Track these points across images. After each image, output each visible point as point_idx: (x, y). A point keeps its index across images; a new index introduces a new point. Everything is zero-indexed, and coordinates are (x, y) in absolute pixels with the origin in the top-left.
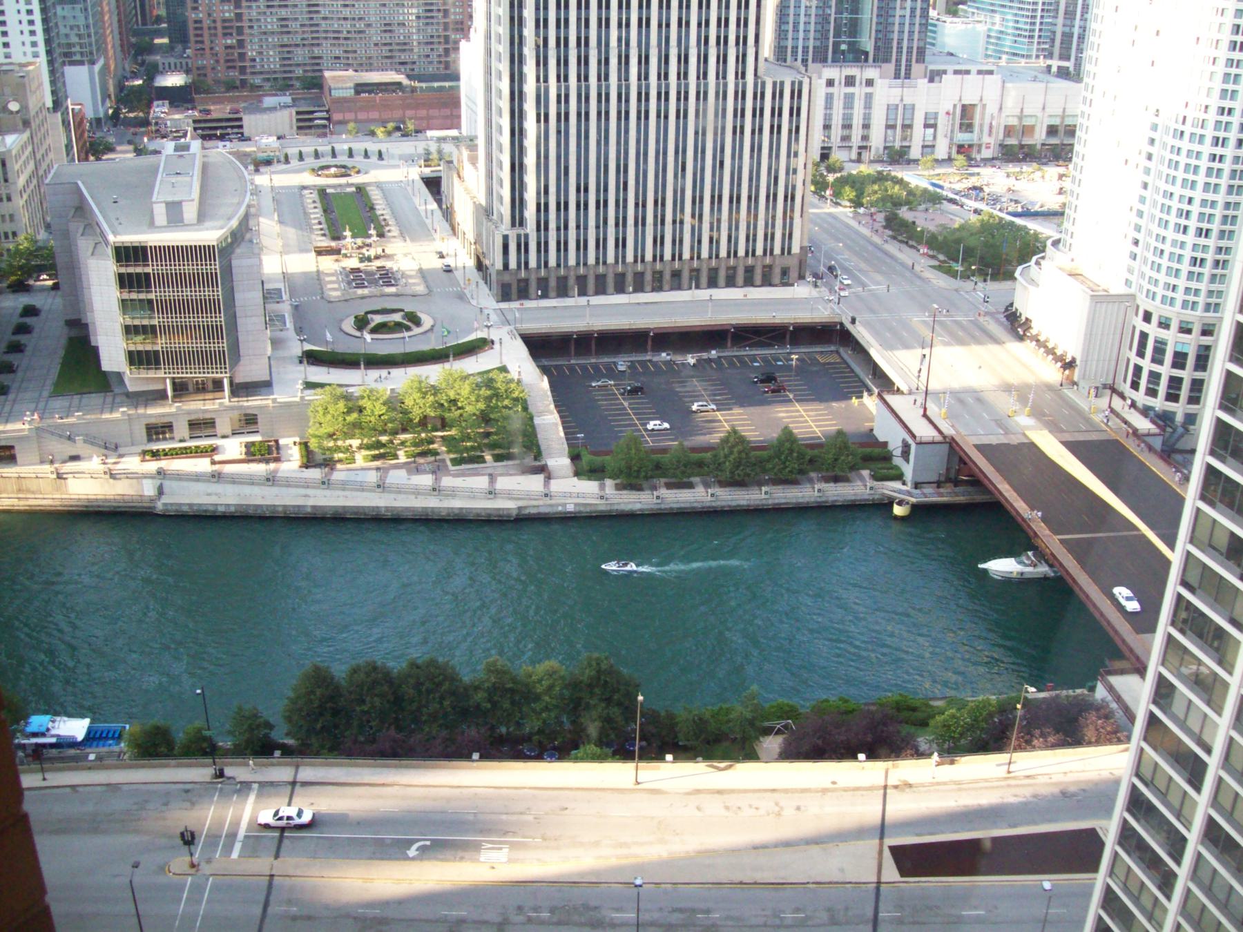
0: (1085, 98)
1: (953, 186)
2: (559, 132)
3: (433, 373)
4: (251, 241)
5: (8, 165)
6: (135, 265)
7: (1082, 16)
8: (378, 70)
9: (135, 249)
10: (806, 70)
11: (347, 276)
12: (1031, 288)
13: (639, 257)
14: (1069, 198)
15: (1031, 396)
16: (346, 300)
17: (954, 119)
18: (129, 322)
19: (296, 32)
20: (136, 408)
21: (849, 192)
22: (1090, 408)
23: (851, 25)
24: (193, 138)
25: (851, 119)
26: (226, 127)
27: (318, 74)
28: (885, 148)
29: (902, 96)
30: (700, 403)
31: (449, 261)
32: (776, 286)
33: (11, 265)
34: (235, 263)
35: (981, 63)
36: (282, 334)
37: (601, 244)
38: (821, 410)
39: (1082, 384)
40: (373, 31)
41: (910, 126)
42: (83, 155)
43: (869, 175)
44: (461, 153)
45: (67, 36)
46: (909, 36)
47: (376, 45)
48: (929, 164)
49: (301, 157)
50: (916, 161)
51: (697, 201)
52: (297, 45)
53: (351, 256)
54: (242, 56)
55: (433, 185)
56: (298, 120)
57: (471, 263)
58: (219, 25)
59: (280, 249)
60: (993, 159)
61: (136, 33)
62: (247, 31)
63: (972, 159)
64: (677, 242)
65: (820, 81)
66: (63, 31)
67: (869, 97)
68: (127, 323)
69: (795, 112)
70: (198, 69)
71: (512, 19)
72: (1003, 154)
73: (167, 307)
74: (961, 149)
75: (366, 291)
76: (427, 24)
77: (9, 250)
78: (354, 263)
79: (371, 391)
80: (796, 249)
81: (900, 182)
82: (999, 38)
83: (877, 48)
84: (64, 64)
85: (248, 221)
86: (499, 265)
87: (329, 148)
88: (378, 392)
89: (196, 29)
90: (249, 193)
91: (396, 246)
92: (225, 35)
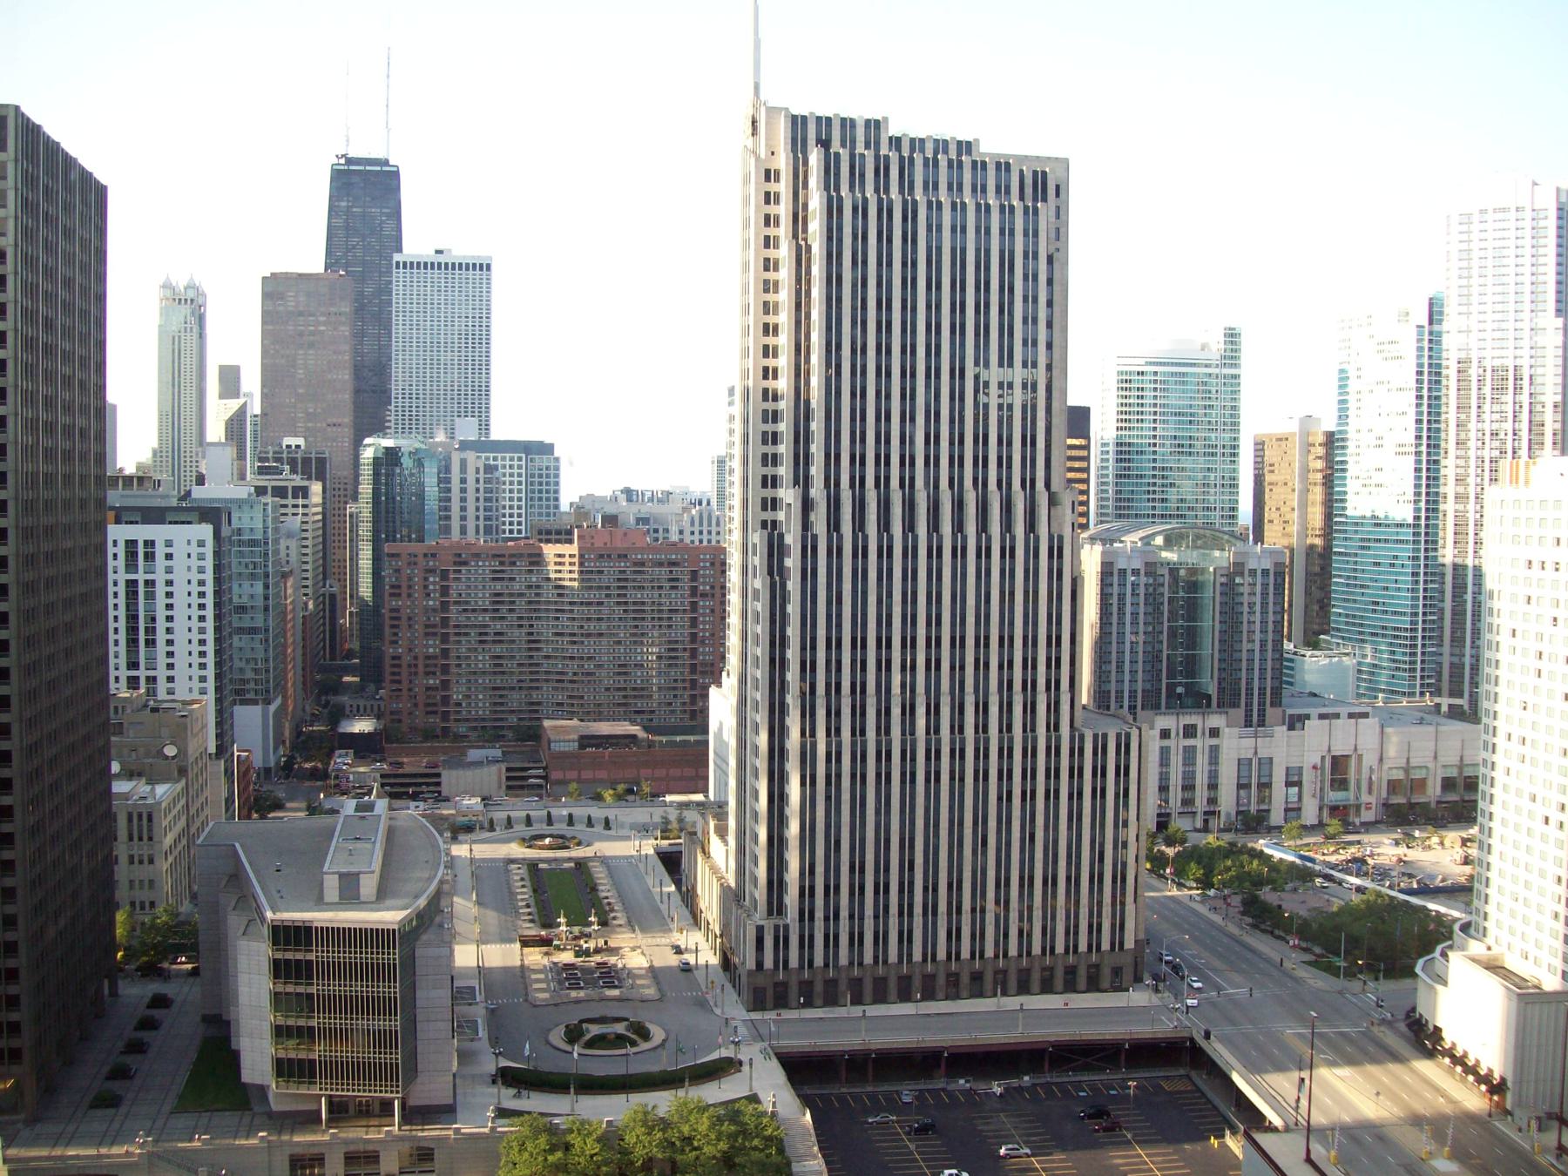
0: (1486, 743)
1: (1327, 858)
2: (828, 798)
3: (663, 1102)
4: (441, 926)
5: (155, 820)
6: (296, 950)
7: (1473, 642)
8: (608, 720)
9: (297, 929)
10: (1135, 719)
11: (559, 974)
12: (1439, 988)
13: (929, 954)
14: (1478, 869)
15: (1450, 1132)
16: (555, 1005)
17: (1323, 774)
18: (281, 1021)
19: (512, 673)
20: (280, 1133)
21: (1195, 870)
22: (1533, 1147)
23: (1187, 663)
24: (379, 796)
25: (1194, 778)
26: (421, 784)
27: (535, 723)
28: (1238, 813)
29: (1256, 748)
30: (1010, 1146)
31: (690, 958)
32: (1105, 991)
33: (143, 944)
34: (418, 953)
35: (1353, 704)
36: (475, 1045)
37: (880, 939)
38: (1169, 1154)
39: (1517, 1113)
40: (604, 673)
41: (1269, 785)
42: (245, 812)
43: (1219, 847)
44: (707, 823)
45: (241, 670)
46: (1261, 674)
47: (607, 689)
48: (1294, 832)
49: (509, 823)
50: (1279, 828)
51: (1003, 883)
52: (513, 688)
53: (565, 949)
54: (446, 700)
55: (671, 862)
56: (508, 778)
57: (714, 960)
58: (421, 663)
59: (476, 936)
60: (1377, 822)
61: (323, 670)
62: (454, 670)
63: (1349, 824)
64: (978, 936)
65: (1152, 733)
66: (238, 664)
67: (1214, 752)
68: (279, 1056)
69: (1123, 771)
70: (392, 713)
71: (772, 660)
72: (1388, 816)
73: (332, 1004)
74: (1335, 810)
75: (582, 994)
76: (670, 665)
77: (143, 924)
78: (567, 957)
79: (583, 1123)
80: (1129, 944)
81: (1260, 855)
82: (1372, 674)
83: (1221, 690)
84: (234, 703)
85: (439, 900)
86: (751, 964)
87: (545, 813)
88: (590, 1125)
89: (394, 666)
90: (442, 867)
91: (623, 939)
92: (427, 674)
